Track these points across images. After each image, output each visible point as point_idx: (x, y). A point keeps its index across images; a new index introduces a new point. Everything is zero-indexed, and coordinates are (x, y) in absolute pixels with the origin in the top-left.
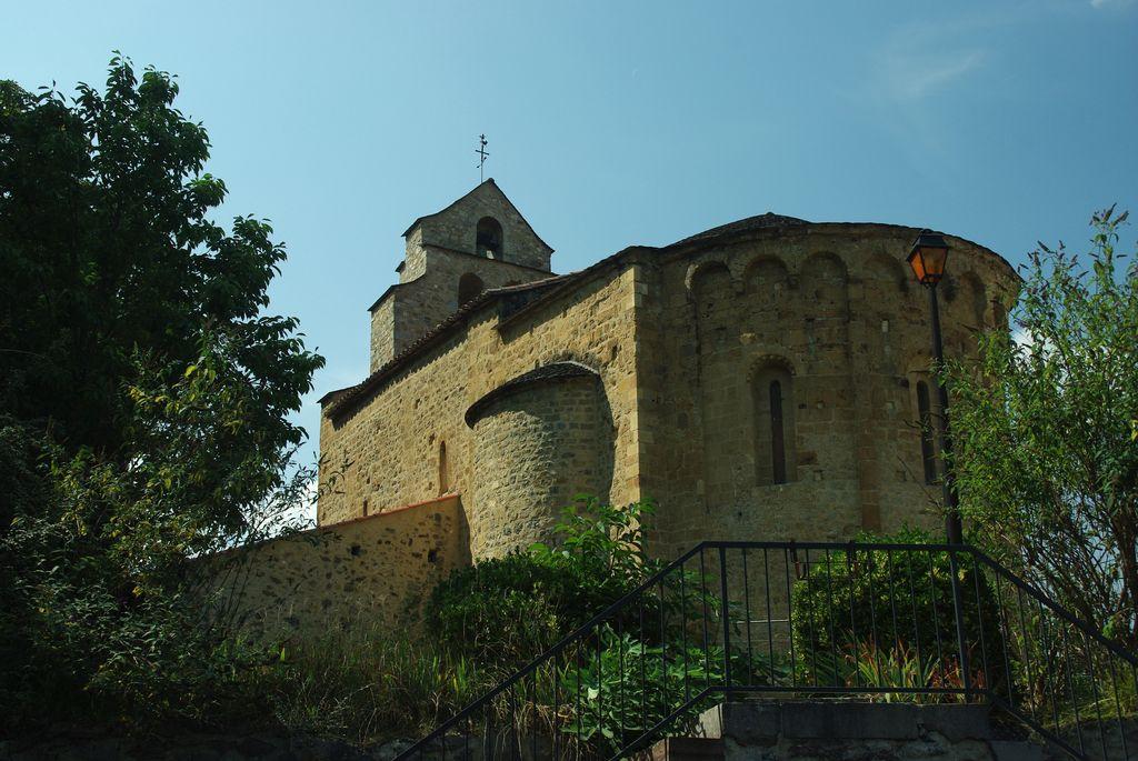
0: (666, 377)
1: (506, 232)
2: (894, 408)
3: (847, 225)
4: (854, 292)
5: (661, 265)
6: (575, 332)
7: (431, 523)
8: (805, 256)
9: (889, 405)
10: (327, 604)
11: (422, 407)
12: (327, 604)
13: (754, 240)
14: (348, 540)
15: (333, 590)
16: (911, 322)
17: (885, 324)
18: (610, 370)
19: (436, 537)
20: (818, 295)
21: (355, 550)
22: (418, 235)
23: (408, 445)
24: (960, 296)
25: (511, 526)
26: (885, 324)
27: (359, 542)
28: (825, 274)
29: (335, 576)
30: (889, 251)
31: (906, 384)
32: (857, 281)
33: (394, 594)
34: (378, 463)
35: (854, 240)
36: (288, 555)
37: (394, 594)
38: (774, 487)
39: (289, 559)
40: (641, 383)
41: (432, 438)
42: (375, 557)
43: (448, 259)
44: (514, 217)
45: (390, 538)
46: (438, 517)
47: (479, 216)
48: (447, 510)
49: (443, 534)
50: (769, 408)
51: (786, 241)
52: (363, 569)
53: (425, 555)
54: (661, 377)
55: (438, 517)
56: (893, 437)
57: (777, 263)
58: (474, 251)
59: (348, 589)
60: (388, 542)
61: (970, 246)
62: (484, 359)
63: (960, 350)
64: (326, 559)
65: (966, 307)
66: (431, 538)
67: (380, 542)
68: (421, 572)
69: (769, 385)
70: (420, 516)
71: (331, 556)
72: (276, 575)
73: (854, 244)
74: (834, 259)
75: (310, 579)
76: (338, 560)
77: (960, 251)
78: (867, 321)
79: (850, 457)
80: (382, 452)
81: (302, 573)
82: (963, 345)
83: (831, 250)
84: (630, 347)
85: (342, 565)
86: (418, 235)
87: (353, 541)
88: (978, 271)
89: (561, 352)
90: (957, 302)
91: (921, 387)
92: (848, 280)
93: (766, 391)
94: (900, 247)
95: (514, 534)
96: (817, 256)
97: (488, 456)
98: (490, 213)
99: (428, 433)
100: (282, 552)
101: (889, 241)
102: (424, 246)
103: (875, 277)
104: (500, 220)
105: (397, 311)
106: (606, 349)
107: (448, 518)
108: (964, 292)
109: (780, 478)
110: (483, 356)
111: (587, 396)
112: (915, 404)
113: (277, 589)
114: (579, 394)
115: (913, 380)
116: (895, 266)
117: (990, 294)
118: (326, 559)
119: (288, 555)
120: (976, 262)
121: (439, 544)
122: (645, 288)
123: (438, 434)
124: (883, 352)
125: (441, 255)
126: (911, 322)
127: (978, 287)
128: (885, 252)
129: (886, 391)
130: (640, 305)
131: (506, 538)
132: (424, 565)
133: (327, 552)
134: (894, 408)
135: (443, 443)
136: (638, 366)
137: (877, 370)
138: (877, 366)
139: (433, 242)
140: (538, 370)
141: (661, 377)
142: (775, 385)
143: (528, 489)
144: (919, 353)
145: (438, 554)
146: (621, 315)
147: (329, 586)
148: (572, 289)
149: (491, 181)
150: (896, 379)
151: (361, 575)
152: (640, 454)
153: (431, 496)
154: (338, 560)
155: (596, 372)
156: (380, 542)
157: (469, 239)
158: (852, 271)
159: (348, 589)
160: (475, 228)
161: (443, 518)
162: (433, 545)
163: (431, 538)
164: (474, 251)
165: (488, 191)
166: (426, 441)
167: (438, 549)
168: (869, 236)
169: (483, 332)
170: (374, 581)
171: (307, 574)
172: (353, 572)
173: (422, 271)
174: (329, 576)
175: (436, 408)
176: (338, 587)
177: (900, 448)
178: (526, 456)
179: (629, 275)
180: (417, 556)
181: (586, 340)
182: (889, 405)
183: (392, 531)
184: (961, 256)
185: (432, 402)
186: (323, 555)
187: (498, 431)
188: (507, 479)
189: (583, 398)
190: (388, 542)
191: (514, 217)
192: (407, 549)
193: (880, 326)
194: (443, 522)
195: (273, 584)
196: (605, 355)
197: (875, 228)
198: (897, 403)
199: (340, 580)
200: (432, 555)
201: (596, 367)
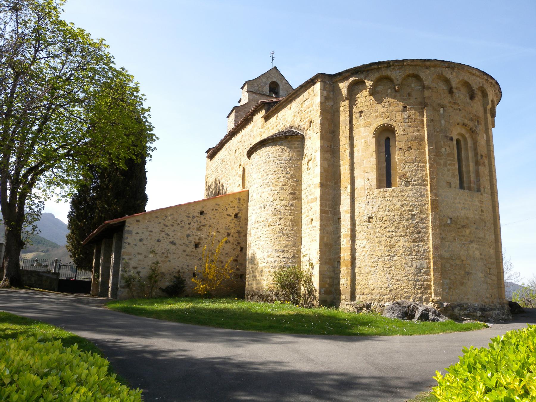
0: (334, 135)
1: (281, 87)
2: (446, 150)
3: (424, 60)
4: (427, 93)
5: (333, 83)
6: (295, 116)
7: (237, 201)
8: (403, 76)
9: (443, 150)
10: (188, 236)
11: (237, 153)
12: (188, 236)
13: (379, 68)
14: (198, 209)
15: (191, 230)
16: (454, 109)
17: (442, 110)
18: (308, 132)
19: (238, 207)
20: (409, 95)
21: (202, 213)
22: (246, 88)
23: (232, 168)
24: (476, 98)
25: (262, 205)
26: (442, 110)
27: (204, 210)
28: (413, 85)
29: (192, 224)
30: (445, 74)
31: (452, 139)
32: (429, 88)
33: (218, 232)
34: (222, 176)
35: (427, 68)
36: (171, 215)
37: (218, 232)
38: (385, 189)
39: (172, 216)
40: (322, 138)
41: (240, 165)
42: (211, 216)
43: (257, 97)
44: (285, 81)
45: (217, 208)
46: (239, 199)
47: (270, 81)
48: (243, 197)
49: (241, 206)
50: (384, 150)
51: (393, 69)
52: (205, 221)
53: (233, 215)
54: (332, 135)
55: (239, 199)
56: (445, 165)
57: (388, 79)
58: (268, 94)
59: (198, 229)
60: (216, 210)
61: (482, 74)
62: (259, 128)
63: (477, 124)
64: (188, 217)
65: (479, 104)
66: (236, 208)
67: (213, 210)
68: (231, 223)
69: (384, 139)
70: (231, 199)
71: (191, 216)
72: (166, 223)
73: (427, 70)
74: (417, 77)
75: (181, 225)
76: (194, 217)
77: (477, 76)
78: (433, 108)
79: (129, 274)
80: (224, 172)
81: (177, 223)
82: (478, 122)
83: (415, 72)
84: (317, 121)
85: (195, 219)
86: (246, 88)
87: (201, 209)
88: (485, 86)
89: (288, 126)
90: (475, 101)
91: (458, 141)
92: (424, 87)
93: (383, 142)
94: (449, 72)
95: (263, 209)
96: (408, 76)
97: (254, 173)
98: (275, 80)
99: (239, 164)
100: (169, 213)
101: (444, 69)
102: (248, 92)
103: (437, 87)
104: (279, 82)
105: (236, 117)
106: (307, 123)
107: (244, 200)
108: (479, 95)
109: (389, 184)
110: (258, 130)
111: (298, 144)
112: (456, 149)
113: (166, 229)
114: (295, 144)
115: (455, 138)
116: (447, 81)
117: (490, 98)
118: (188, 217)
119: (171, 215)
120: (484, 82)
121: (240, 210)
122: (325, 93)
123: (242, 164)
124: (441, 123)
125: (254, 95)
126: (454, 109)
127: (485, 95)
128: (442, 75)
129: (442, 142)
130: (323, 101)
131: (259, 211)
132: (232, 220)
133: (189, 214)
134: (446, 150)
135: (244, 168)
136: (321, 130)
137: (438, 132)
138: (438, 130)
139: (251, 90)
140: (279, 133)
141: (332, 135)
142: (388, 139)
143: (269, 188)
144: (458, 124)
145: (239, 215)
146: (314, 106)
147: (189, 228)
148: (293, 96)
149: (275, 68)
150: (447, 137)
151: (204, 224)
152: (321, 172)
153: (240, 189)
154: (194, 217)
155: (302, 133)
156: (213, 210)
157: (266, 89)
158: (426, 83)
159: (198, 229)
160: (268, 85)
161: (242, 199)
162: (237, 211)
163: (236, 208)
164: (268, 94)
165: (274, 71)
166: (238, 167)
167: (239, 213)
168: (435, 66)
169: (259, 117)
170: (210, 226)
171: (180, 223)
172: (200, 222)
173: (247, 101)
174: (189, 224)
175: (242, 153)
176: (194, 229)
177: (448, 170)
178: (269, 173)
179: (318, 86)
180: (230, 215)
181: (299, 119)
182: (443, 150)
183: (218, 205)
184: (478, 79)
185: (240, 151)
186: (187, 215)
187: (258, 161)
188: (261, 183)
189: (296, 145)
190: (216, 210)
191: (285, 81)
192: (225, 213)
193: (439, 111)
194: (242, 201)
195: (164, 227)
196: (307, 125)
197: (437, 63)
198: (448, 148)
199: (194, 225)
200: (236, 215)
201: (303, 131)
